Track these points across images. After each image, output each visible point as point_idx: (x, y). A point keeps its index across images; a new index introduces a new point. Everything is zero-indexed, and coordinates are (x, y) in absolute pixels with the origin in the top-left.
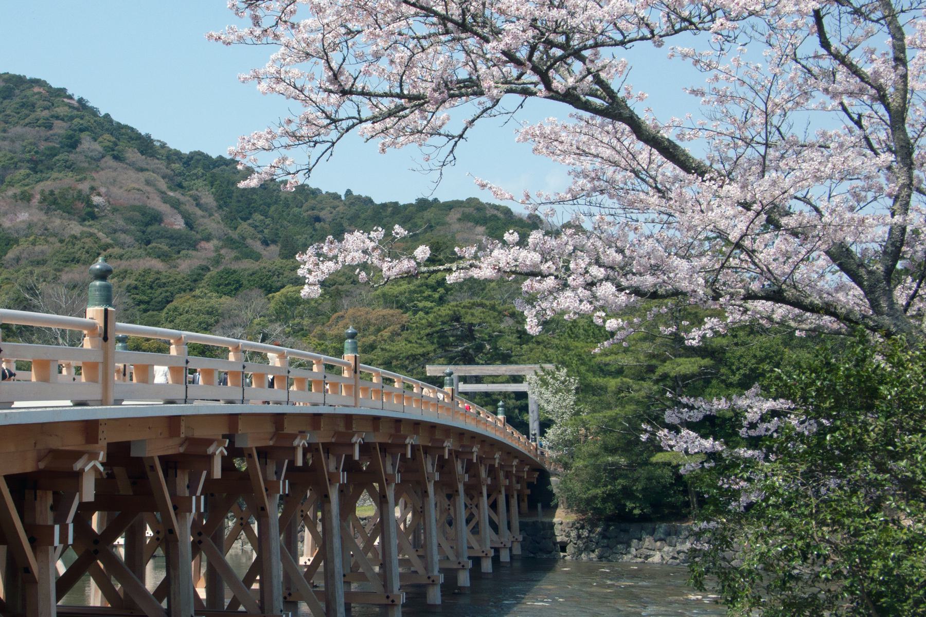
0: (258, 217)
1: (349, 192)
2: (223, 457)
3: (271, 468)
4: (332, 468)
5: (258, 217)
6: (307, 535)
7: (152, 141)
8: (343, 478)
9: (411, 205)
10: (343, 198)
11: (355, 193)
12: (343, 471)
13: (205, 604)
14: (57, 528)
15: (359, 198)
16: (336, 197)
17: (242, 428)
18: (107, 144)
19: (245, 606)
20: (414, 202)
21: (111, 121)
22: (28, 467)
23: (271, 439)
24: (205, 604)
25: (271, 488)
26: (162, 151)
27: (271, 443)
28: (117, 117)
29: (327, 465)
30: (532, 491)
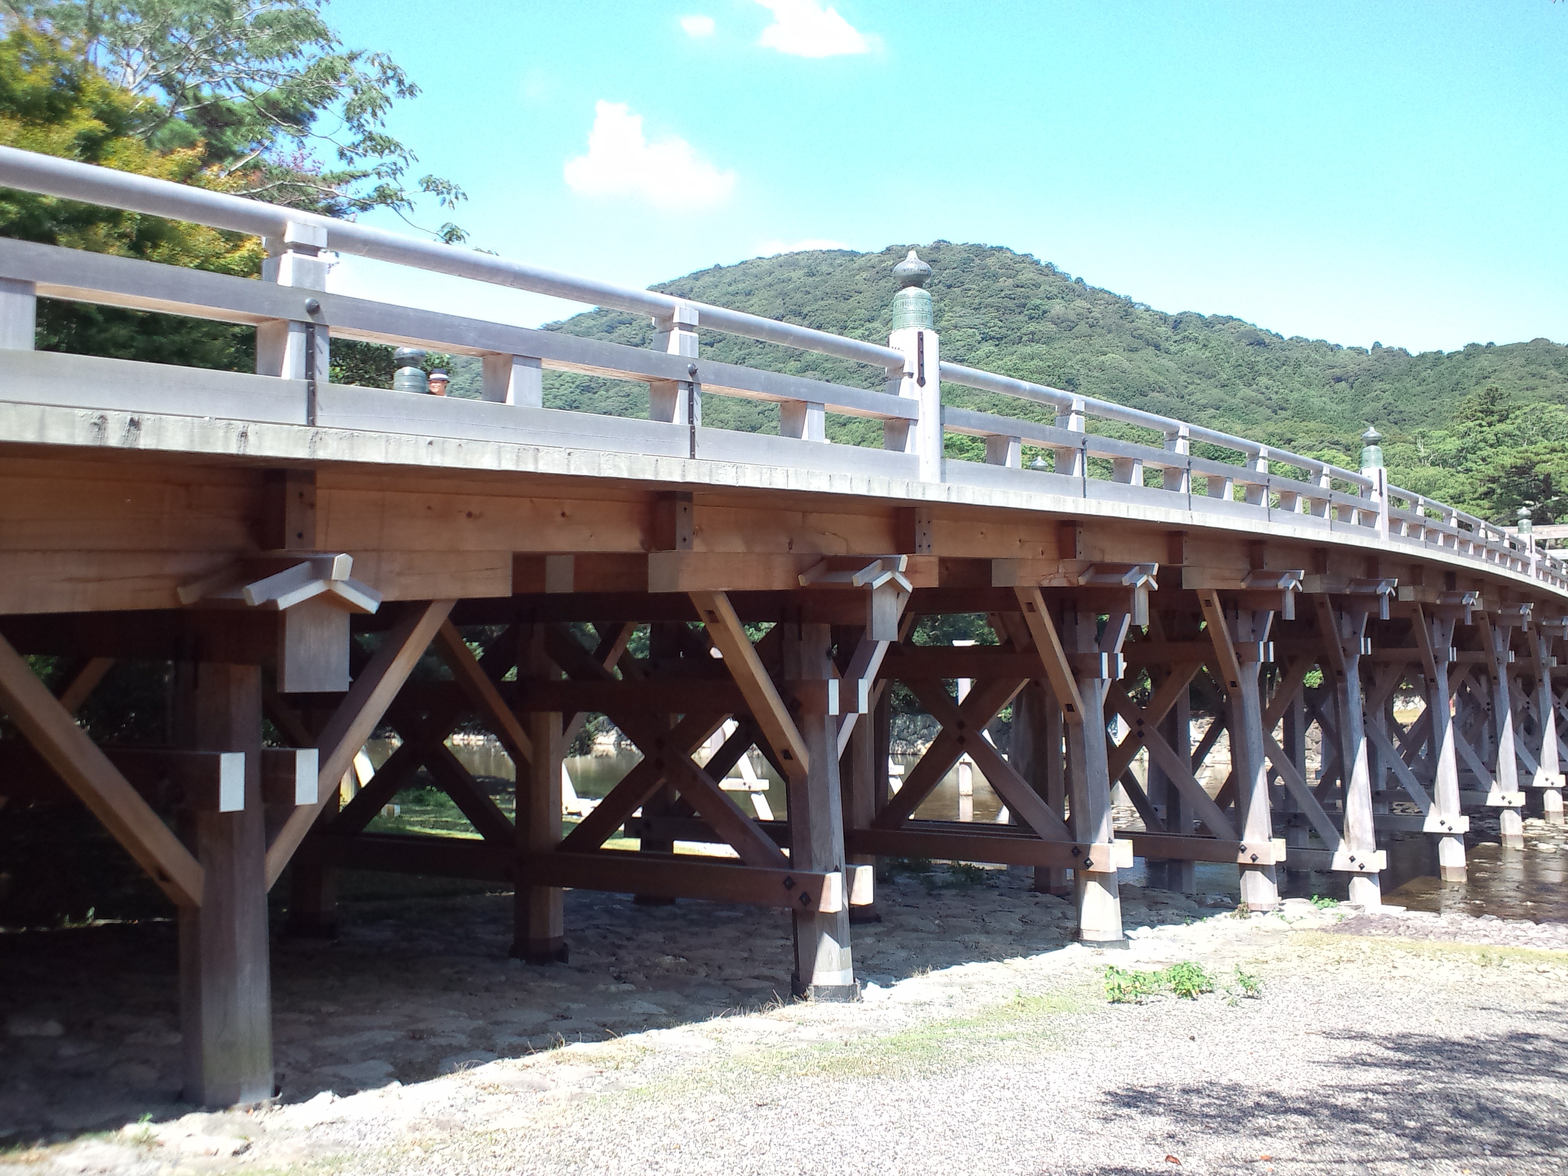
0: (1264, 381)
1: (1377, 345)
2: (1152, 594)
3: (1244, 627)
4: (1347, 631)
5: (1264, 381)
6: (1477, 875)
7: (1132, 305)
8: (1366, 646)
9: (1459, 352)
10: (1370, 353)
11: (1385, 345)
12: (1366, 637)
13: (341, 809)
14: (834, 687)
15: (1390, 351)
16: (1360, 351)
17: (1188, 558)
18: (1079, 310)
19: (700, 812)
20: (1462, 349)
21: (1084, 287)
22: (1059, 582)
23: (1242, 580)
24: (341, 809)
25: (1245, 656)
26: (1146, 315)
27: (1243, 586)
28: (1091, 281)
29: (1340, 630)
30: (1391, 859)
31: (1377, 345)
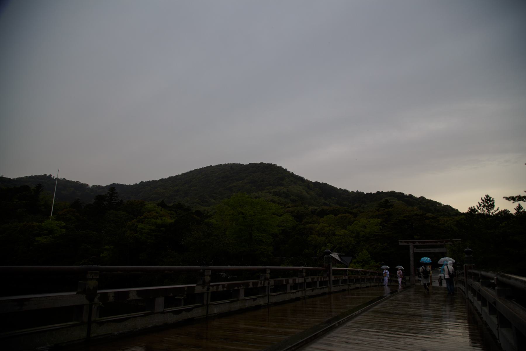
1: (357, 191)
31: (357, 191)
